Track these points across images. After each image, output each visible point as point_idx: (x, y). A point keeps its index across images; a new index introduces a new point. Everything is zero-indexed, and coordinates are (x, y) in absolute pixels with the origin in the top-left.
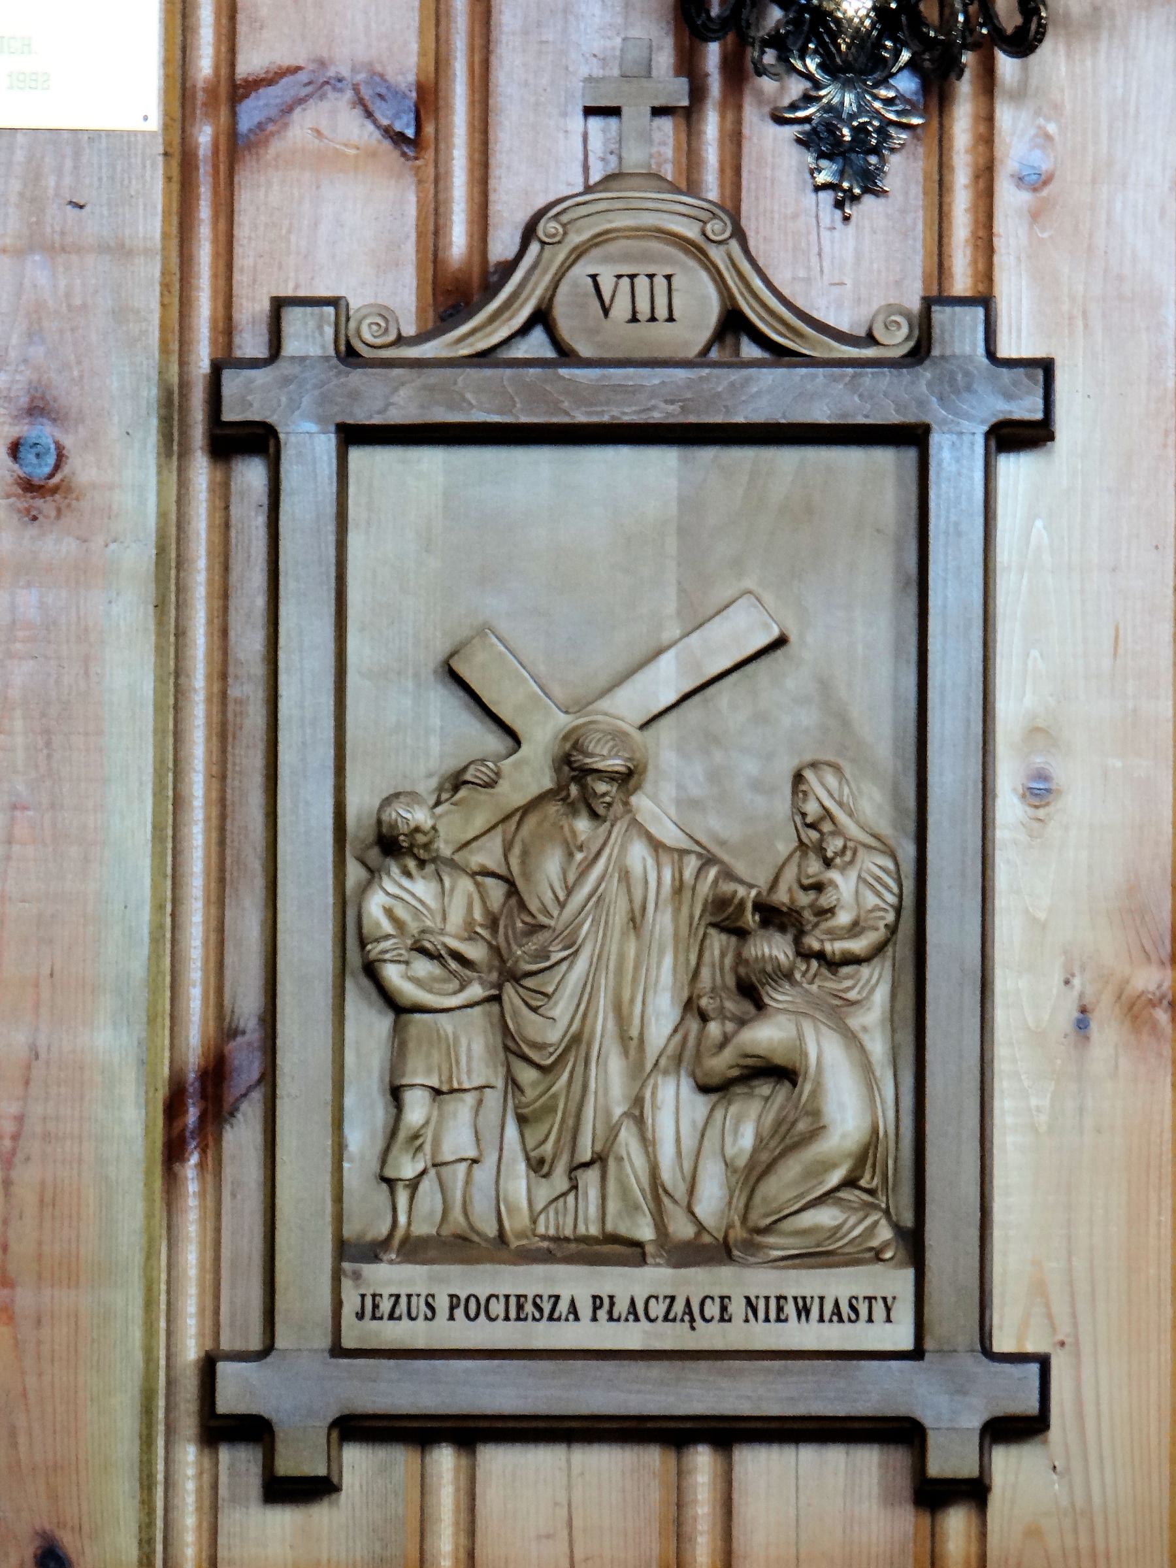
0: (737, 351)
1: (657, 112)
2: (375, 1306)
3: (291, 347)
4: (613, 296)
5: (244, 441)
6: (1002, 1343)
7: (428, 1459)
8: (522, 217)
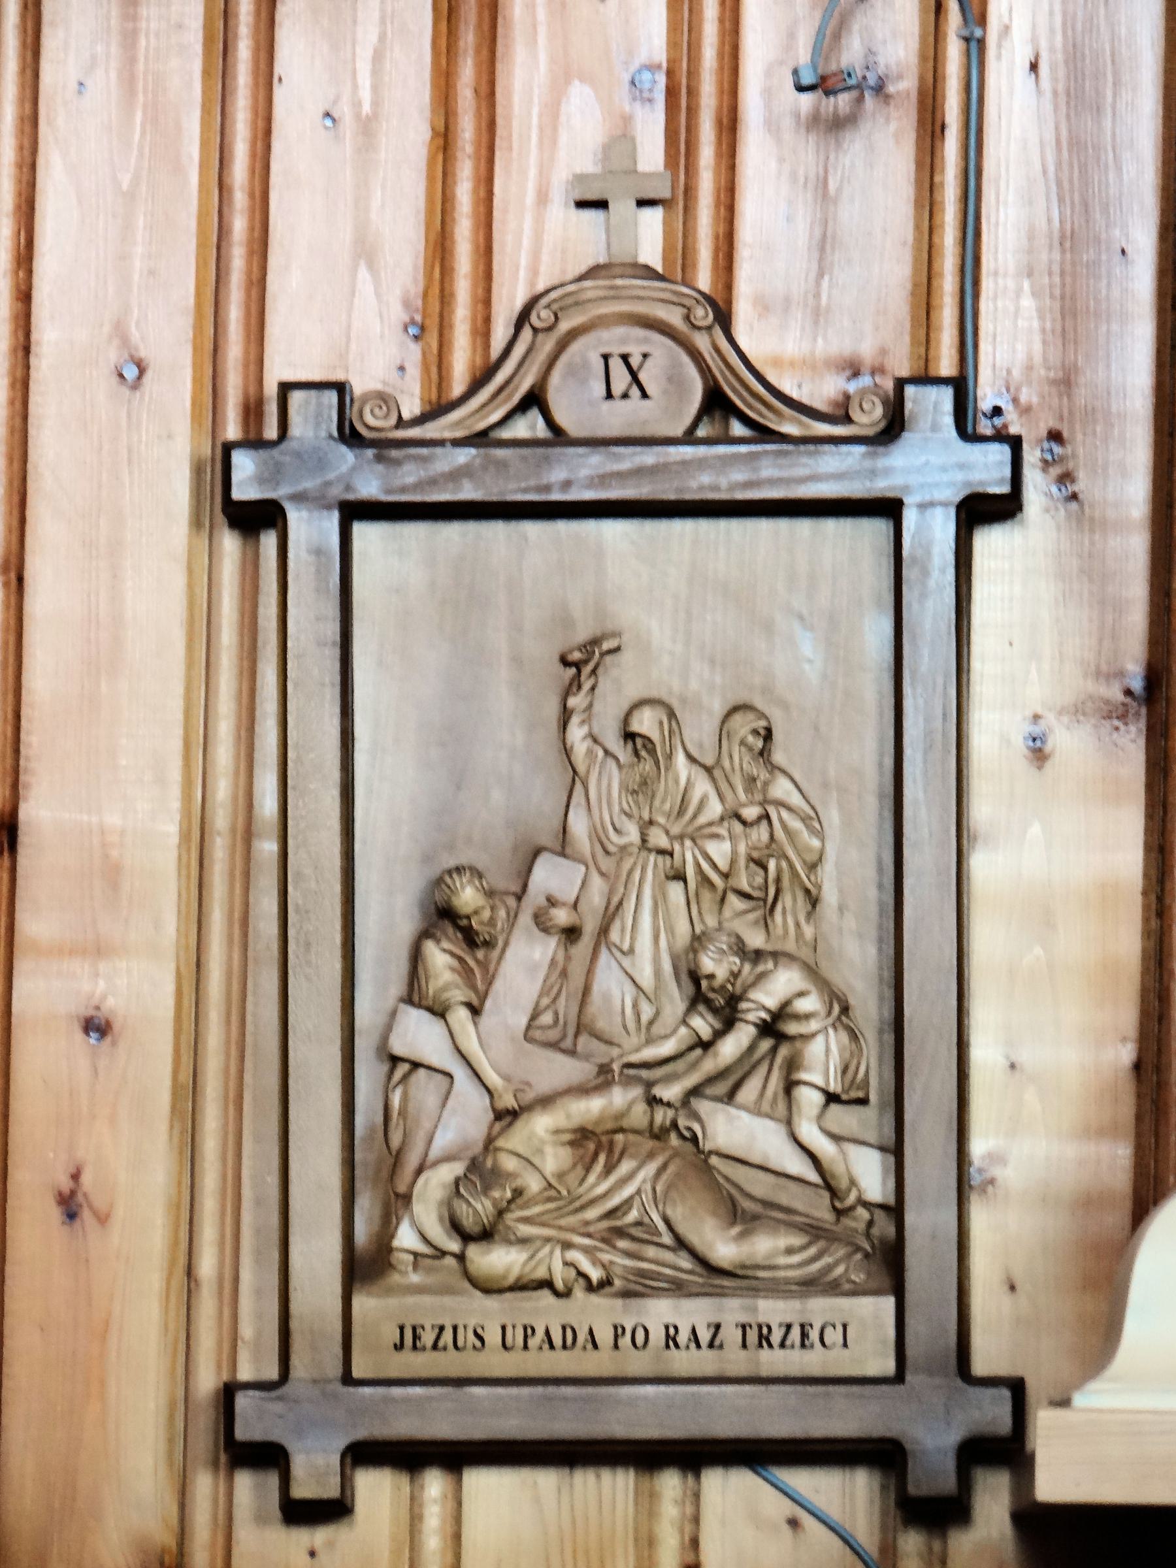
0: (727, 426)
1: (642, 203)
2: (416, 1337)
3: (297, 428)
5: (256, 519)
6: (980, 1366)
8: (519, 303)
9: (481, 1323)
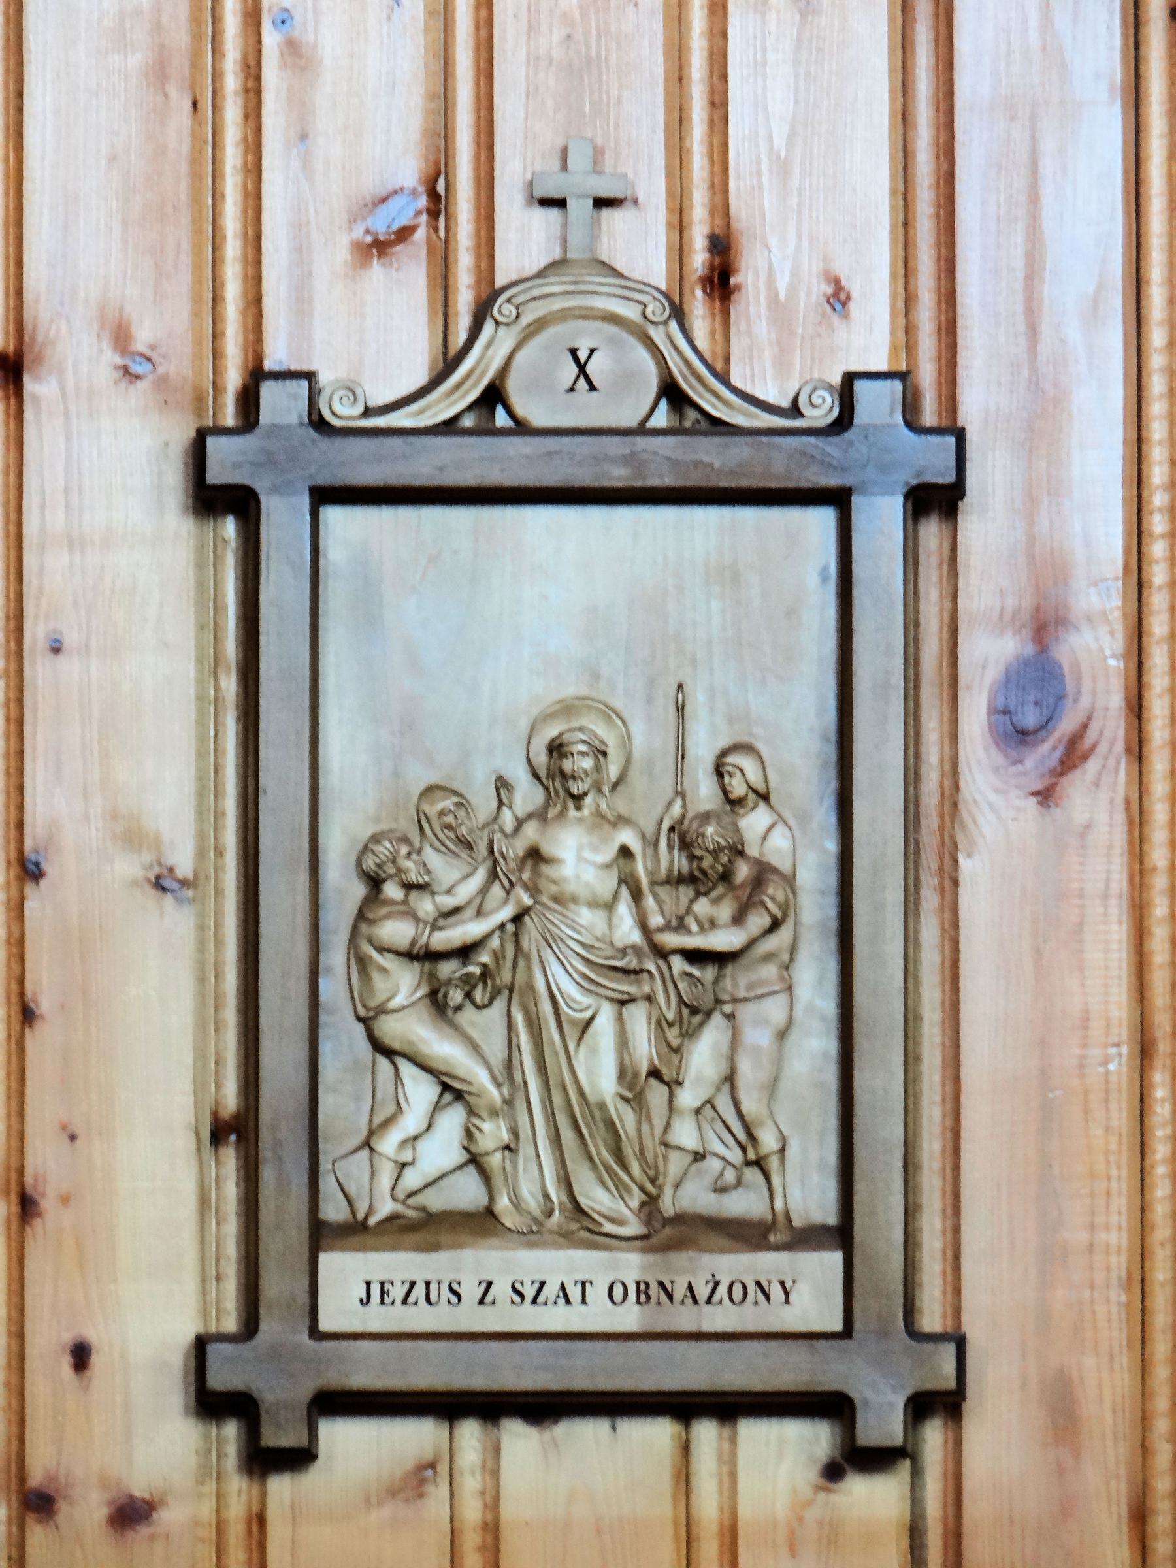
4: (681, 294)
7: (457, 1433)
9: (391, 1278)
